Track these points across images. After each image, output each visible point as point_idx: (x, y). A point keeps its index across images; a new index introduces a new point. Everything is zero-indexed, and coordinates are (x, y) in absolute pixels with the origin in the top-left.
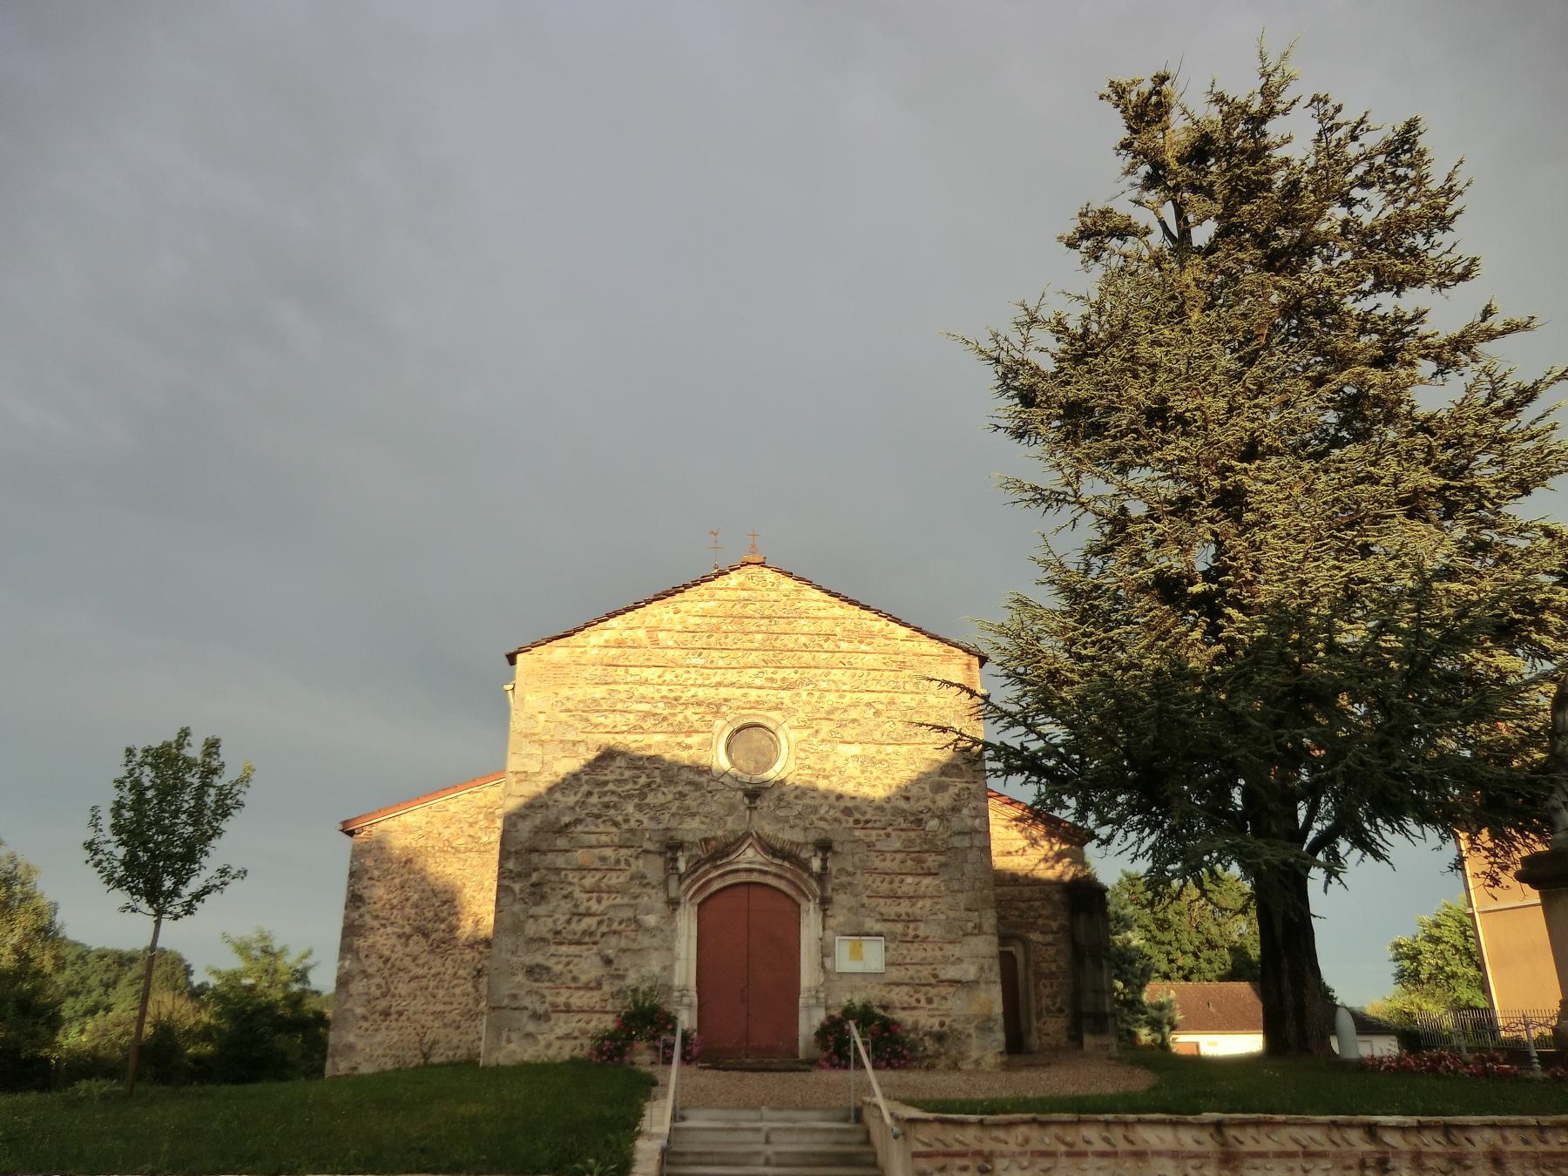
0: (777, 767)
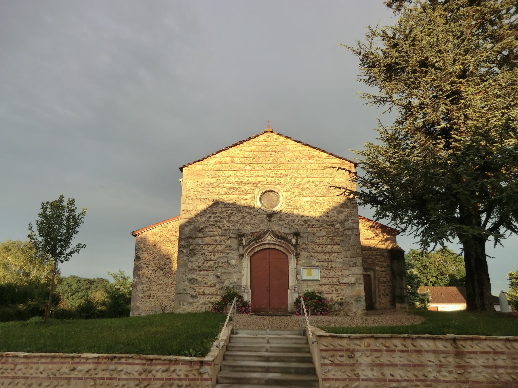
0: (279, 206)
